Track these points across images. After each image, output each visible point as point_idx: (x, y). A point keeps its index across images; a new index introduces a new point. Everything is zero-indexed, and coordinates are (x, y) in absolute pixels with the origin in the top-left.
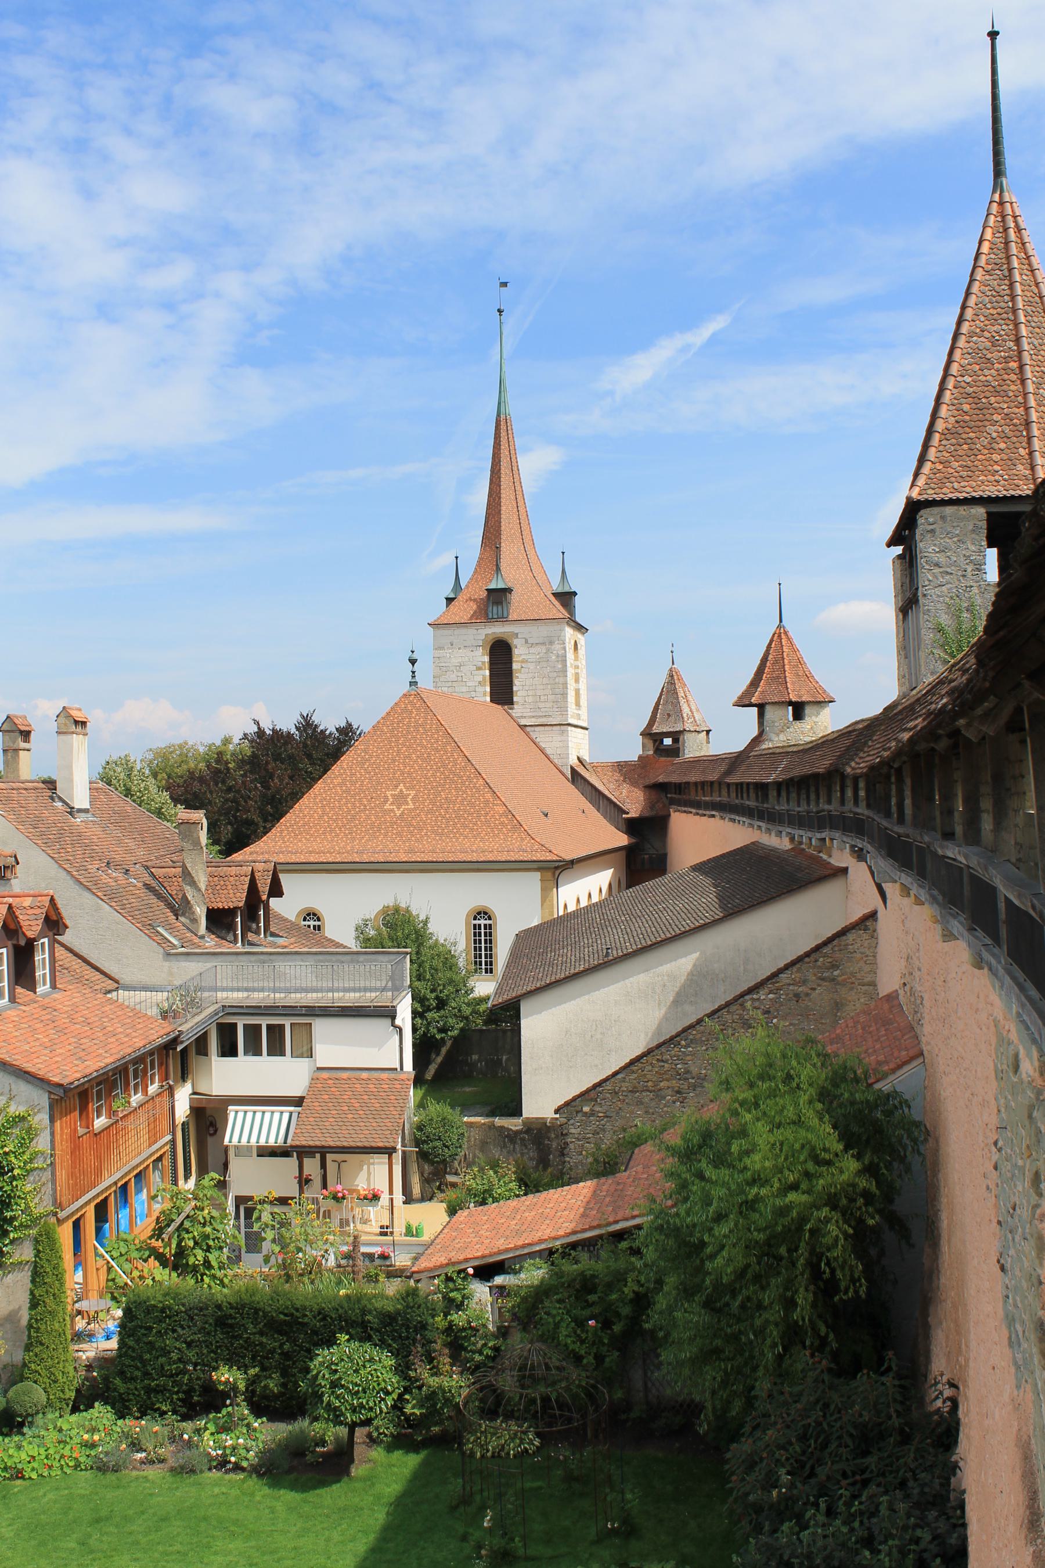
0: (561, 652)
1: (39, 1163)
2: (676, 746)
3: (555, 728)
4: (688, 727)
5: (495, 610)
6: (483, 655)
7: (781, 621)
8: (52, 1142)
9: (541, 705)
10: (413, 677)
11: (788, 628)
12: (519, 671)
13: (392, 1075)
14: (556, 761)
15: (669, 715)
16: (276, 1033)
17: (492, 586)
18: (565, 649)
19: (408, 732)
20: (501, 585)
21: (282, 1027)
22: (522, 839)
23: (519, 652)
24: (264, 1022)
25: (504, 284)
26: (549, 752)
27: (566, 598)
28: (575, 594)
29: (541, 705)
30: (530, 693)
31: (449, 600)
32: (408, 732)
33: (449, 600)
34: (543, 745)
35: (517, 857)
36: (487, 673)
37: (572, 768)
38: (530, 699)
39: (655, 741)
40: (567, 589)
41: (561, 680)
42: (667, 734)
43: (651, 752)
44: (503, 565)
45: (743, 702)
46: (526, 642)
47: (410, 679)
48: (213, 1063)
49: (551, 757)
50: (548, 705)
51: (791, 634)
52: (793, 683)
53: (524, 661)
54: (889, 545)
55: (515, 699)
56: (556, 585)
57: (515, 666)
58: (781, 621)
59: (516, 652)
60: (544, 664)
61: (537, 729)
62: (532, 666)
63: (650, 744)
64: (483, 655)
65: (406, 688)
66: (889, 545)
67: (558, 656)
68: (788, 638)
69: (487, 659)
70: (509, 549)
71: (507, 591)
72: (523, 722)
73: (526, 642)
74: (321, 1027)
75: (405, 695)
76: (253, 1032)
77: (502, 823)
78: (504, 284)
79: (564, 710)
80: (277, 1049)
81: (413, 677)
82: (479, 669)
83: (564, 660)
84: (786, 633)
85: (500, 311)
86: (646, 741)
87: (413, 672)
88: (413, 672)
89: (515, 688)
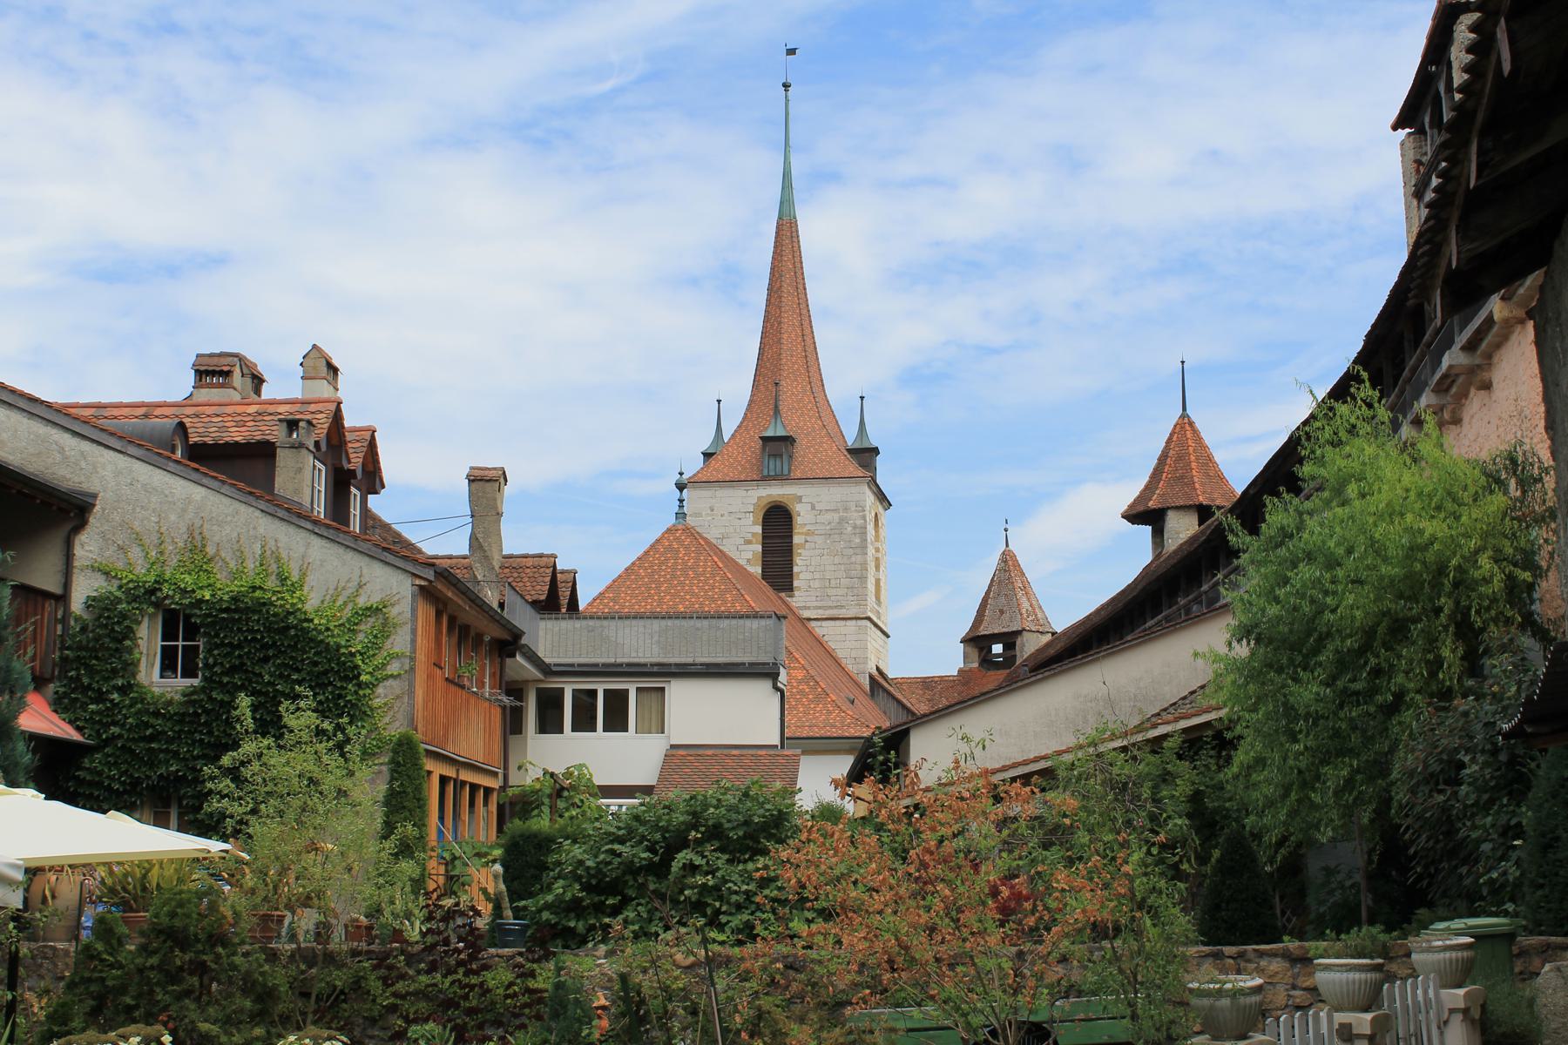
0: (859, 522)
1: (394, 668)
2: (1011, 653)
3: (849, 623)
4: (1028, 625)
5: (773, 466)
6: (754, 523)
7: (1184, 408)
8: (413, 641)
9: (831, 592)
10: (681, 507)
11: (1193, 418)
12: (802, 546)
13: (772, 752)
14: (850, 667)
15: (1002, 612)
16: (617, 702)
17: (770, 433)
18: (864, 518)
19: (674, 577)
20: (781, 432)
21: (624, 694)
22: (829, 713)
23: (803, 517)
24: (600, 687)
25: (791, 52)
26: (840, 654)
27: (865, 455)
28: (876, 451)
29: (831, 592)
30: (817, 576)
31: (707, 455)
32: (674, 577)
33: (707, 455)
34: (832, 645)
35: (822, 733)
36: (759, 548)
37: (871, 677)
38: (816, 584)
39: (981, 650)
40: (866, 445)
41: (859, 558)
42: (996, 638)
43: (976, 665)
44: (783, 407)
45: (1136, 515)
46: (813, 508)
47: (676, 509)
48: (529, 741)
49: (844, 662)
50: (840, 592)
51: (1198, 425)
52: (1202, 484)
53: (809, 533)
54: (1395, 128)
55: (796, 583)
56: (851, 437)
57: (797, 539)
58: (1184, 408)
59: (799, 521)
60: (837, 537)
61: (825, 623)
62: (820, 540)
63: (974, 654)
64: (754, 523)
65: (673, 520)
66: (1395, 128)
67: (855, 527)
68: (1195, 432)
69: (759, 529)
70: (791, 390)
71: (788, 440)
72: (806, 614)
73: (813, 508)
74: (679, 694)
75: (669, 531)
76: (584, 703)
77: (801, 692)
78: (791, 52)
79: (861, 599)
80: (616, 721)
81: (681, 507)
82: (749, 542)
83: (864, 533)
84: (1191, 424)
85: (786, 86)
86: (970, 649)
87: (681, 501)
88: (681, 501)
89: (796, 569)
